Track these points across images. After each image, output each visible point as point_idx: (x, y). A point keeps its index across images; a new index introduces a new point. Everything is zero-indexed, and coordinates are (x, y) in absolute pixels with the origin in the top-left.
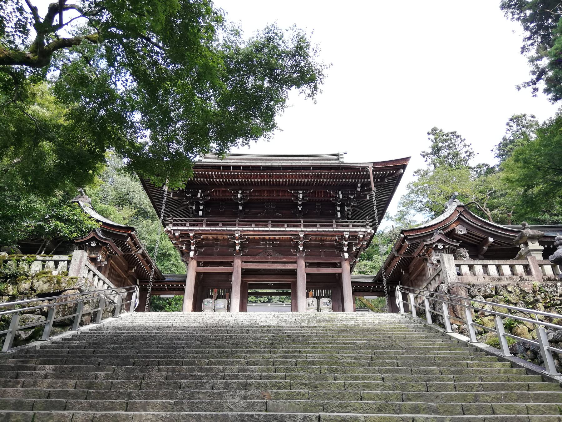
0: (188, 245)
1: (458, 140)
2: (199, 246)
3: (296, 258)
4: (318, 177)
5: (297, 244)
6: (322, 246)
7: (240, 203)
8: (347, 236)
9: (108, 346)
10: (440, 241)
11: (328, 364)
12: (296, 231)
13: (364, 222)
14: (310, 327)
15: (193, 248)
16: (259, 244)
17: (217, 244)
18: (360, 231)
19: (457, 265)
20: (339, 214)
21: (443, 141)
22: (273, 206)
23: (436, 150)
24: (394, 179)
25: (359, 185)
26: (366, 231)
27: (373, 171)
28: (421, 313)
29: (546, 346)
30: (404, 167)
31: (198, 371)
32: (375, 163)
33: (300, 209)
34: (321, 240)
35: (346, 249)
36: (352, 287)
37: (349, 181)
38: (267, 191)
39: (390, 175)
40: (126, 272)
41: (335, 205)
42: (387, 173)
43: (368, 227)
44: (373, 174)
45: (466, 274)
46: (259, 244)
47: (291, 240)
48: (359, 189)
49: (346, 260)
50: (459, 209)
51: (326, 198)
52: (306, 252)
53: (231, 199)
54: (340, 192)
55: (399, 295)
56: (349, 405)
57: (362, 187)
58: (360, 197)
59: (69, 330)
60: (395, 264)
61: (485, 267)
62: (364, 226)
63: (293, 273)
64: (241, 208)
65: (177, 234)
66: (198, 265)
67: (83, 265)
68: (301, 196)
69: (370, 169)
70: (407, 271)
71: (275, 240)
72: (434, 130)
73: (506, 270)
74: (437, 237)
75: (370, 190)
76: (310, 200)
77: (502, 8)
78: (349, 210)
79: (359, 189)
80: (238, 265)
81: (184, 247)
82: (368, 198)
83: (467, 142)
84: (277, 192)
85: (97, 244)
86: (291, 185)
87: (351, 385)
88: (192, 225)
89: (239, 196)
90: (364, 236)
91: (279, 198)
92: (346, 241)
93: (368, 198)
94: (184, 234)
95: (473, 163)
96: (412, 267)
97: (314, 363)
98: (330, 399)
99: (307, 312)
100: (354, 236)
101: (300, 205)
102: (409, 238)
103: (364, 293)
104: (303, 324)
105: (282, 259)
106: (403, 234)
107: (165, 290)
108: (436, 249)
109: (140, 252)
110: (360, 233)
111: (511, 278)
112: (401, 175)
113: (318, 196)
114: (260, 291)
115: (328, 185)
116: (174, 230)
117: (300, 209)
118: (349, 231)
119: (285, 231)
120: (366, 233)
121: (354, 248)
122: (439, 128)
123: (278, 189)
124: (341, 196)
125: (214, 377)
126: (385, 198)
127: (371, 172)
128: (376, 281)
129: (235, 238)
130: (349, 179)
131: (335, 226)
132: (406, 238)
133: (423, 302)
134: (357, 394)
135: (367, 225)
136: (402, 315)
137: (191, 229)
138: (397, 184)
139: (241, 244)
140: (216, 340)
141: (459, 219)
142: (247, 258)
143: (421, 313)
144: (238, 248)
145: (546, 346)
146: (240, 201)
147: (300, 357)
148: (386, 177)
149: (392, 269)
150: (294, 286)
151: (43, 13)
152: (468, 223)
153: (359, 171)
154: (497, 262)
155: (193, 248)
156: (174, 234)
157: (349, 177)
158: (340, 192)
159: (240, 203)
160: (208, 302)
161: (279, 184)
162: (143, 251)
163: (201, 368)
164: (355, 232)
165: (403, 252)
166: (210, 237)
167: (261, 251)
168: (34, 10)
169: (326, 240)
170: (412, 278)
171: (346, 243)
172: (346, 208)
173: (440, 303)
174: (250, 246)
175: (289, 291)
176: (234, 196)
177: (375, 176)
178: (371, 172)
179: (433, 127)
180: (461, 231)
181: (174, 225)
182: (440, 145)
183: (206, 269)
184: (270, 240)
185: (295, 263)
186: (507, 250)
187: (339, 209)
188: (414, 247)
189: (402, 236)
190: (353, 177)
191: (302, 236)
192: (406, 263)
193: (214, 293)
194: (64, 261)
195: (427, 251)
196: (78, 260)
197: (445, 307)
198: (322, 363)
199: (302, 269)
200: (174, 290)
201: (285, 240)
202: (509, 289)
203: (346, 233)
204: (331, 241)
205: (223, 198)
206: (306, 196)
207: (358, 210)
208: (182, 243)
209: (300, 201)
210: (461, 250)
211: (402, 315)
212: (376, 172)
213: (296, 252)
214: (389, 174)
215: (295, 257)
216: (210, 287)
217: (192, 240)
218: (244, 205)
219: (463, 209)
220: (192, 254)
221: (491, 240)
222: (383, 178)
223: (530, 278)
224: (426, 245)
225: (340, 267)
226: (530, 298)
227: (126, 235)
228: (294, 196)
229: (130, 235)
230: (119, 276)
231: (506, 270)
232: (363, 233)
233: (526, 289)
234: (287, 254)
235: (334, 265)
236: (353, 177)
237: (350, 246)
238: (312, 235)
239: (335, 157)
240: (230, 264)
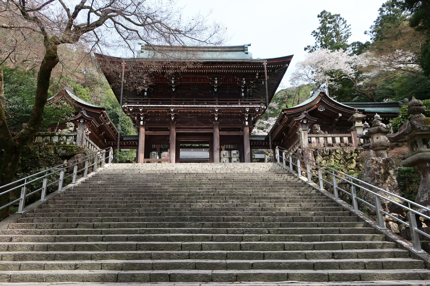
0: (139, 116)
1: (342, 22)
2: (146, 117)
3: (213, 126)
5: (213, 117)
6: (231, 117)
7: (173, 86)
8: (248, 110)
9: (111, 186)
10: (305, 118)
11: (230, 195)
12: (213, 107)
14: (221, 174)
16: (187, 116)
17: (158, 116)
18: (257, 107)
19: (309, 137)
20: (243, 94)
21: (329, 23)
23: (324, 29)
24: (281, 70)
25: (257, 74)
26: (261, 107)
27: (267, 65)
28: (288, 164)
29: (335, 186)
30: (289, 63)
31: (165, 199)
32: (268, 60)
33: (216, 90)
34: (230, 113)
35: (247, 119)
36: (250, 143)
38: (192, 78)
39: (278, 68)
40: (98, 135)
42: (276, 66)
43: (262, 104)
44: (267, 67)
45: (314, 142)
46: (187, 116)
47: (209, 113)
48: (257, 77)
49: (247, 126)
50: (321, 95)
52: (219, 121)
53: (167, 83)
54: (244, 79)
55: (277, 151)
56: (237, 213)
58: (258, 82)
59: (82, 177)
60: (279, 130)
61: (326, 138)
62: (259, 104)
63: (211, 135)
64: (174, 90)
66: (146, 130)
67: (84, 138)
68: (216, 82)
69: (265, 64)
70: (287, 133)
71: (198, 112)
72: (314, 31)
73: (338, 140)
74: (303, 116)
75: (264, 78)
76: (222, 84)
77: (325, 17)
78: (250, 91)
79: (257, 77)
80: (174, 132)
81: (136, 118)
82: (263, 83)
83: (348, 24)
85: (84, 121)
86: (209, 73)
87: (239, 205)
88: (140, 103)
89: (173, 82)
90: (259, 110)
92: (247, 114)
93: (263, 83)
94: (136, 109)
95: (349, 41)
97: (222, 195)
98: (229, 211)
100: (252, 110)
101: (216, 88)
103: (258, 147)
104: (217, 172)
107: (124, 145)
108: (302, 123)
109: (109, 123)
110: (256, 109)
111: (340, 145)
112: (287, 68)
115: (235, 74)
116: (129, 107)
117: (216, 90)
118: (249, 107)
119: (206, 107)
120: (261, 109)
121: (252, 118)
122: (328, 11)
123: (200, 76)
124: (244, 82)
125: (174, 202)
126: (276, 82)
127: (265, 66)
129: (171, 112)
130: (250, 70)
131: (239, 104)
132: (285, 114)
133: (289, 158)
134: (241, 208)
135: (262, 102)
136: (278, 164)
137: (141, 106)
138: (284, 73)
139: (175, 116)
140: (169, 182)
141: (321, 101)
143: (288, 164)
144: (173, 118)
145: (335, 186)
146: (173, 85)
147: (215, 192)
148: (276, 69)
149: (277, 133)
150: (211, 143)
151: (72, 11)
152: (326, 104)
153: (256, 65)
154: (333, 135)
156: (129, 110)
157: (251, 69)
158: (244, 79)
159: (173, 86)
160: (154, 154)
162: (111, 123)
163: (166, 198)
164: (253, 107)
165: (283, 122)
166: (154, 111)
167: (188, 120)
168: (68, 10)
169: (233, 113)
170: (289, 138)
171: (247, 115)
172: (248, 90)
173: (297, 160)
174: (181, 117)
175: (208, 145)
176: (169, 81)
177: (268, 69)
178: (265, 66)
179: (322, 11)
180: (321, 109)
181: (128, 103)
182: (328, 25)
184: (195, 112)
185: (212, 128)
186: (344, 125)
187: (243, 90)
188: (289, 122)
189: (283, 113)
190: (253, 69)
192: (286, 129)
194: (72, 136)
195: (297, 124)
196: (81, 135)
197: (299, 162)
198: (226, 195)
199: (217, 134)
200: (130, 146)
201: (205, 113)
202: (337, 151)
204: (237, 113)
205: (161, 82)
206: (220, 82)
208: (135, 115)
209: (216, 85)
210: (316, 125)
211: (278, 164)
212: (269, 66)
213: (213, 121)
214: (280, 65)
216: (155, 146)
217: (141, 113)
218: (175, 87)
220: (142, 123)
221: (340, 115)
222: (274, 69)
223: (351, 144)
224: (296, 121)
225: (243, 131)
226: (349, 157)
227: (100, 113)
228: (211, 81)
229: (102, 113)
230: (95, 138)
231: (338, 140)
232: (258, 109)
233: (347, 151)
235: (239, 130)
236: (253, 69)
237: (250, 117)
238: (224, 110)
239: (242, 49)
240: (169, 130)
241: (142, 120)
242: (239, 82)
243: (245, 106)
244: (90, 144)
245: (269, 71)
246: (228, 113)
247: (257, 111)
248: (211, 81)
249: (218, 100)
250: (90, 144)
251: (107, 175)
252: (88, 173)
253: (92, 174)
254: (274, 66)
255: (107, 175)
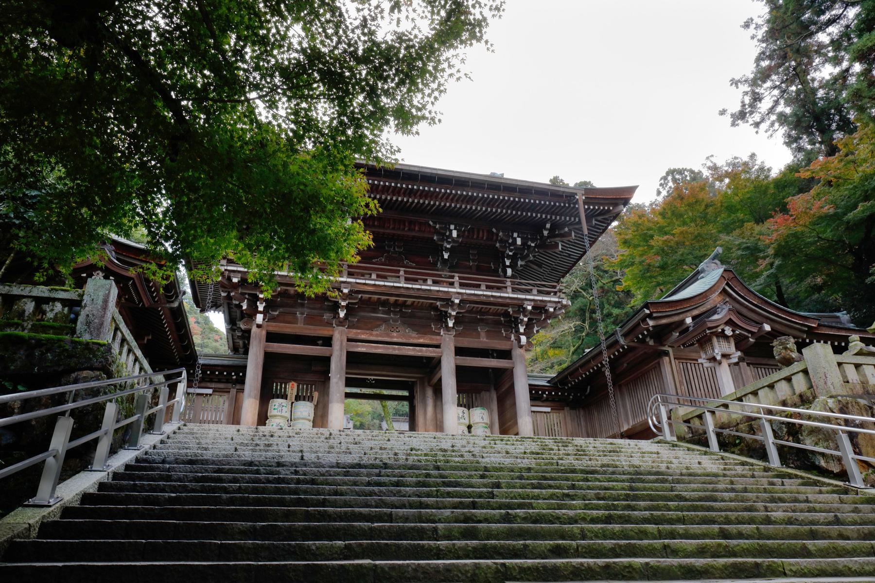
4: (491, 203)
13: (554, 287)
15: (261, 308)
18: (550, 302)
20: (509, 272)
22: (399, 247)
25: (548, 226)
33: (446, 256)
36: (530, 392)
37: (537, 216)
41: (503, 256)
51: (490, 243)
57: (551, 230)
63: (431, 366)
65: (235, 280)
69: (580, 197)
84: (410, 223)
91: (413, 234)
92: (525, 316)
96: (625, 365)
99: (458, 428)
101: (447, 250)
102: (655, 315)
105: (419, 338)
106: (648, 309)
113: (478, 236)
114: (385, 392)
117: (446, 256)
118: (533, 300)
128: (555, 384)
142: (353, 333)
155: (261, 308)
161: (420, 210)
172: (520, 263)
183: (285, 348)
184: (396, 303)
191: (457, 301)
193: (292, 389)
196: (100, 302)
203: (529, 303)
207: (535, 267)
215: (438, 337)
219: (732, 276)
234: (422, 328)
241: (260, 312)
242: (501, 241)
243: (523, 297)
244: (125, 349)
245: (577, 220)
246: (477, 312)
247: (551, 310)
248: (437, 232)
249: (460, 278)
250: (125, 349)
251: (184, 462)
252: (113, 451)
253: (126, 457)
254: (594, 208)
255: (184, 462)
